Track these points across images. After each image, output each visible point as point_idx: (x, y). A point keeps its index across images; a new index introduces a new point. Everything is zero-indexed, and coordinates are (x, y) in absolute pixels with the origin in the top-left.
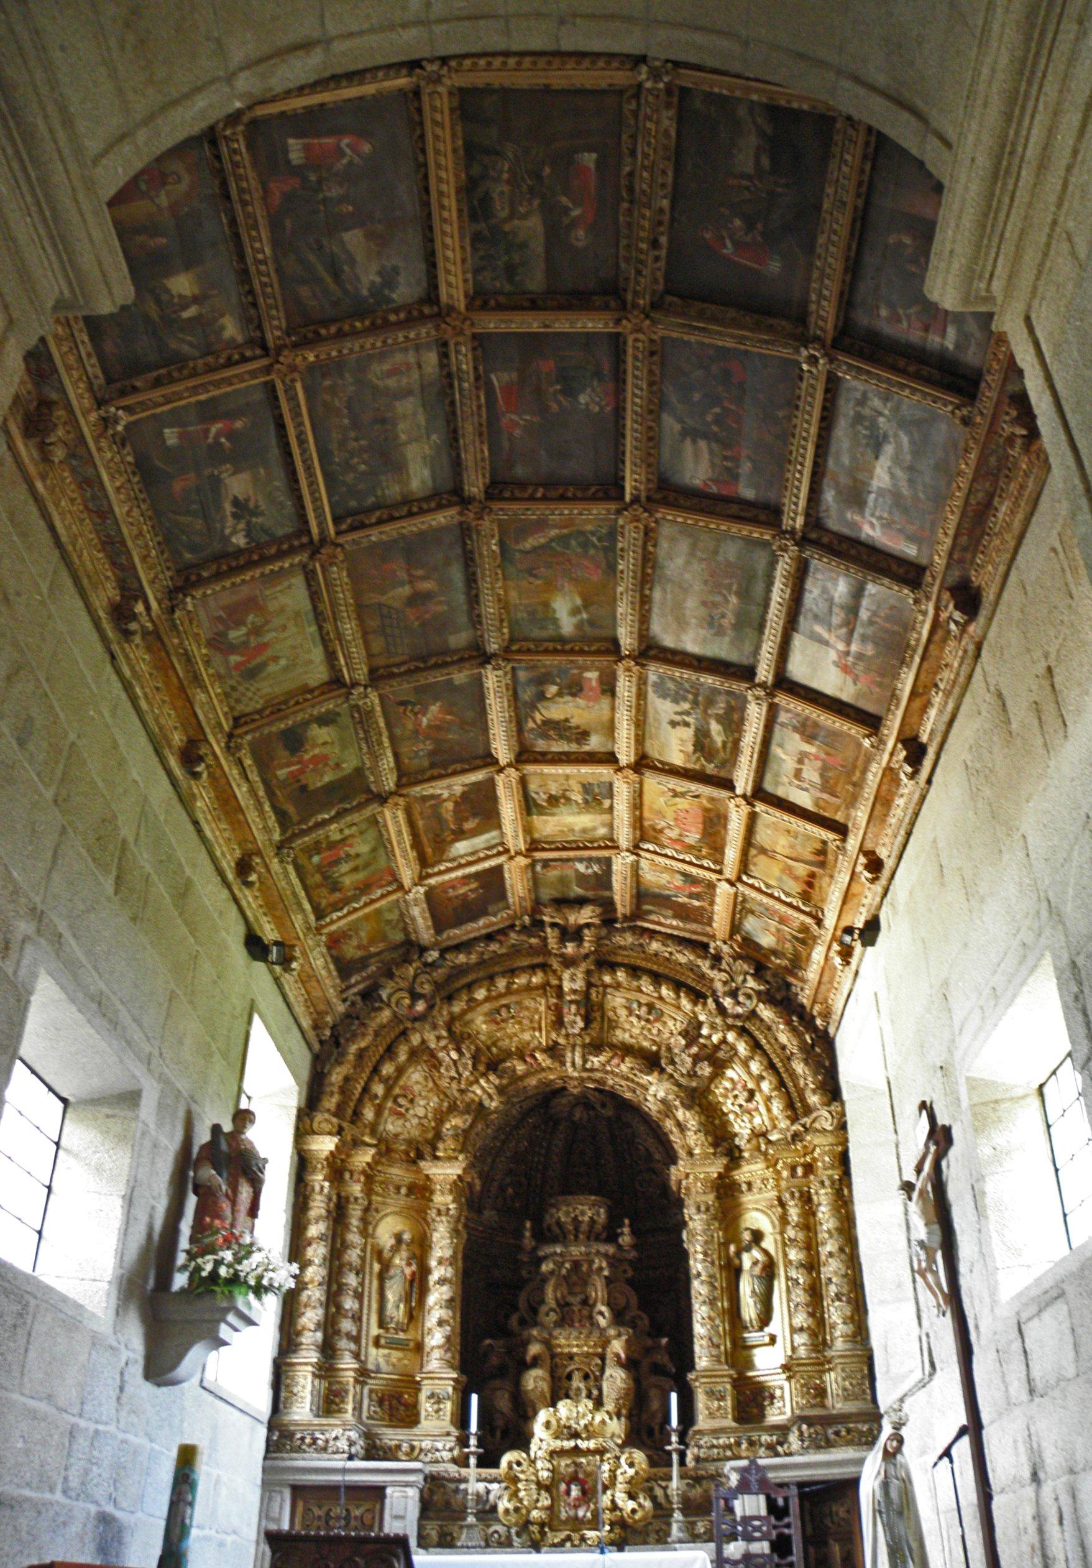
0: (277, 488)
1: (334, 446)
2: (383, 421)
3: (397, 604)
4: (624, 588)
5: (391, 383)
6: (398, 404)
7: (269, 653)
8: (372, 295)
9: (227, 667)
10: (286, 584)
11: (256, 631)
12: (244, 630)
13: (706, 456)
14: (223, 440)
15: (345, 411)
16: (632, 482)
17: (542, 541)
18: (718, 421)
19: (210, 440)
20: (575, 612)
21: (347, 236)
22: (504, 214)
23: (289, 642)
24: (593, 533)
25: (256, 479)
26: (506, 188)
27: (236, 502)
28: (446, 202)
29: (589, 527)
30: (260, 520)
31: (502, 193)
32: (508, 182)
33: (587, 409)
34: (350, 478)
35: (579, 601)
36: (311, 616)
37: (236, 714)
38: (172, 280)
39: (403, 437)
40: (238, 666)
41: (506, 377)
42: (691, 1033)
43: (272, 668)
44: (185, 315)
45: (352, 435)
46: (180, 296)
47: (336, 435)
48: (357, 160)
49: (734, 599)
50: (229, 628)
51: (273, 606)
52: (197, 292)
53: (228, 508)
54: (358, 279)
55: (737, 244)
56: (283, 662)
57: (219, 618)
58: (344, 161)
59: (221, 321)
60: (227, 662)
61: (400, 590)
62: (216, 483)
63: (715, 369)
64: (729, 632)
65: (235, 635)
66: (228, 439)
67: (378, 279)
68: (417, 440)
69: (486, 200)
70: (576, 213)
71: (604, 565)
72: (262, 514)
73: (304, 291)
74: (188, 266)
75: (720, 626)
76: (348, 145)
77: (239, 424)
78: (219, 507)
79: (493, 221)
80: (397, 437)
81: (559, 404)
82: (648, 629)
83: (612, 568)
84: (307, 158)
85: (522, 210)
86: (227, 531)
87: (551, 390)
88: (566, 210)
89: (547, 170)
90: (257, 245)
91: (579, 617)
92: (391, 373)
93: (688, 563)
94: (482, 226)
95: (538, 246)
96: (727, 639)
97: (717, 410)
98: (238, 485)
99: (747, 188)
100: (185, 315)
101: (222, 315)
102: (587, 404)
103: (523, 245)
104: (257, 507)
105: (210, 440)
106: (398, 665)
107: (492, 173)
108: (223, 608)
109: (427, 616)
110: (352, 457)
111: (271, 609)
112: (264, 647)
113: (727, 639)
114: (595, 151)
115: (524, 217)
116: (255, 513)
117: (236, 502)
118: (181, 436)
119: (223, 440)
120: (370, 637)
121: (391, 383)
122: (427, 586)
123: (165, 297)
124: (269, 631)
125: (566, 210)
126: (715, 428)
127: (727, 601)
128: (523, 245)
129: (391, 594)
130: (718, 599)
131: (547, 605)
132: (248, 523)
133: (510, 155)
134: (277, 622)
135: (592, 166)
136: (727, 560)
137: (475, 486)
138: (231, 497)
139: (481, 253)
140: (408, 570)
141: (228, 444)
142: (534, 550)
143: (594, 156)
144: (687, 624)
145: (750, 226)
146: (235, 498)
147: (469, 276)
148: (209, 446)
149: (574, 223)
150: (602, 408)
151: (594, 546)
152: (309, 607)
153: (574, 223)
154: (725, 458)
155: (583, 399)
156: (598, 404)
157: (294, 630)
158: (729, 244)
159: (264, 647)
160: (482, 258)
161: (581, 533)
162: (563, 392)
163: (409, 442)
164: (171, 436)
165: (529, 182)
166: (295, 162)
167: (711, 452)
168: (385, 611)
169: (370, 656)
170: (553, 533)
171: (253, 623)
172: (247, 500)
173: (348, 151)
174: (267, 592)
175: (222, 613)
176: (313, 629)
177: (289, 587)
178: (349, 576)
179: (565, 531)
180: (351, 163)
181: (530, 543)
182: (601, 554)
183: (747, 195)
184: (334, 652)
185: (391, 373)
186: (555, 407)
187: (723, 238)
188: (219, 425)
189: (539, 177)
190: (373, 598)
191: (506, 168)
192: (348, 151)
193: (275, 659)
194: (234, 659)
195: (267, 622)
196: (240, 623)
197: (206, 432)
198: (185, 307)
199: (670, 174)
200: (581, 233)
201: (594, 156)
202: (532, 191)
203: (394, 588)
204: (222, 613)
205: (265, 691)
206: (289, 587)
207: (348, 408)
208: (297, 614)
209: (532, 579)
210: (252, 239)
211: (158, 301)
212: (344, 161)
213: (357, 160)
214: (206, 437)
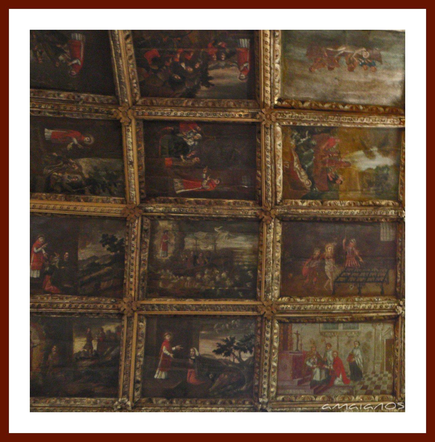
0: (218, 327)
1: (203, 288)
2: (195, 257)
3: (338, 271)
4: (347, 123)
5: (171, 249)
6: (187, 247)
7: (345, 361)
8: (115, 251)
9: (343, 387)
10: (294, 336)
11: (321, 363)
12: (317, 371)
13: (220, 71)
14: (174, 349)
15: (182, 278)
16: (239, 114)
17: (303, 173)
18: (190, 63)
19: (171, 355)
20: (370, 155)
21: (81, 257)
22: (80, 177)
23: (342, 345)
24: (298, 141)
25: (207, 337)
26: (66, 175)
27: (218, 352)
28: (65, 207)
29: (293, 143)
30: (237, 341)
31: (69, 177)
32: (63, 173)
33: (199, 141)
34: (228, 283)
35: (361, 153)
36: (329, 326)
37: (389, 391)
38: (74, 349)
39: (210, 248)
40: (345, 380)
41: (179, 185)
42: (285, 117)
43: (359, 360)
44: (95, 348)
45: (199, 276)
46: (84, 348)
47: (197, 285)
48: (44, 246)
49: (342, 49)
50: (311, 379)
51: (307, 348)
52: (85, 339)
53: (221, 357)
54: (104, 257)
55: (74, 58)
56: (358, 352)
57: (300, 383)
58: (44, 252)
59: (105, 331)
60: (339, 386)
61: (327, 268)
62: (201, 359)
63: (156, 68)
64: (375, 52)
65: (318, 376)
66: (174, 346)
67: (107, 246)
68: (215, 239)
69: (71, 184)
70: (75, 141)
71: (326, 135)
72: (233, 340)
73: (104, 285)
74: (71, 341)
75: (370, 58)
76: (37, 249)
77: (167, 338)
78: (218, 361)
79: (83, 183)
80: (209, 252)
81: (193, 157)
82: (385, 107)
83: (329, 130)
84: (38, 270)
85: (77, 168)
86: (236, 361)
87: (184, 160)
88: (74, 146)
89: (55, 154)
90: (61, 305)
91: (376, 154)
92: (165, 249)
93: (316, 80)
94: (86, 189)
95: (96, 162)
96: (383, 53)
97: (183, 65)
98: (206, 348)
99: (41, 53)
100: (95, 348)
101: (102, 330)
102: (195, 140)
103: (95, 168)
104: (227, 341)
105: (171, 355)
106: (396, 278)
107: (59, 181)
108: (294, 376)
109: (357, 253)
110: (214, 279)
111: (308, 350)
112: (337, 362)
113: (383, 53)
114: (44, 130)
115: (80, 167)
116: (230, 343)
117: (218, 352)
118: (162, 370)
119: (174, 349)
120: (364, 291)
121: (171, 249)
122: (330, 249)
123: (83, 355)
124: (325, 355)
125: (74, 146)
126: (197, 66)
127: (344, 54)
128: (95, 168)
129: (328, 274)
130: (343, 60)
131: (362, 174)
132: (236, 348)
133: (50, 171)
134: (321, 349)
135: (51, 131)
136: (307, 55)
137: (248, 210)
138: (214, 354)
139: (101, 191)
140: (313, 259)
141: (177, 347)
142: (310, 178)
143: (46, 130)
144: (374, 80)
145: (61, 51)
146: (215, 351)
147: (112, 199)
148: (175, 357)
149: (81, 142)
150: (199, 132)
151: (309, 140)
152: (321, 325)
153: (81, 142)
154: (219, 59)
155: (190, 143)
156: (195, 134)
157: (334, 339)
158: (75, 62)
159: (337, 362)
160: (104, 191)
161: (297, 149)
162: (185, 154)
163: (215, 245)
164: (160, 375)
165: (62, 163)
166: (39, 275)
167: (217, 67)
168: (342, 279)
169: (382, 294)
170: (296, 166)
171: (314, 363)
172: (219, 345)
173: (39, 249)
174: (295, 348)
175: (297, 380)
176: (341, 326)
177: (297, 334)
178: (301, 297)
179: (295, 158)
180: (45, 249)
181: (304, 180)
182: (316, 136)
183: (44, 53)
184: (366, 318)
185: (165, 249)
186: (196, 160)
187: (73, 65)
188: (164, 348)
189: (58, 159)
190: (330, 283)
191: (56, 174)
192: (39, 249)
193: (352, 356)
194: (338, 381)
195: (318, 355)
196: (310, 371)
197: (165, 355)
198: (91, 347)
199: (49, 92)
200: (86, 139)
201: (46, 130)
202: (66, 163)
203: (323, 271)
204: (297, 380)
205: (377, 368)
206: (297, 334)
207: (180, 275)
208: (322, 334)
209: (338, 182)
210: (58, 307)
211: (83, 359)
212: (44, 252)
213: (44, 246)
214: (169, 356)
